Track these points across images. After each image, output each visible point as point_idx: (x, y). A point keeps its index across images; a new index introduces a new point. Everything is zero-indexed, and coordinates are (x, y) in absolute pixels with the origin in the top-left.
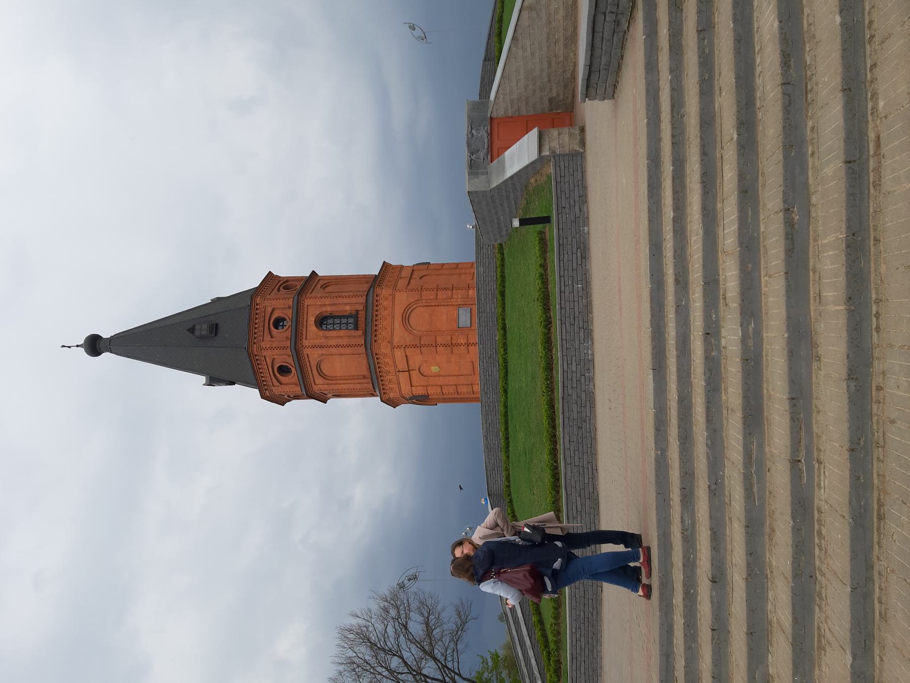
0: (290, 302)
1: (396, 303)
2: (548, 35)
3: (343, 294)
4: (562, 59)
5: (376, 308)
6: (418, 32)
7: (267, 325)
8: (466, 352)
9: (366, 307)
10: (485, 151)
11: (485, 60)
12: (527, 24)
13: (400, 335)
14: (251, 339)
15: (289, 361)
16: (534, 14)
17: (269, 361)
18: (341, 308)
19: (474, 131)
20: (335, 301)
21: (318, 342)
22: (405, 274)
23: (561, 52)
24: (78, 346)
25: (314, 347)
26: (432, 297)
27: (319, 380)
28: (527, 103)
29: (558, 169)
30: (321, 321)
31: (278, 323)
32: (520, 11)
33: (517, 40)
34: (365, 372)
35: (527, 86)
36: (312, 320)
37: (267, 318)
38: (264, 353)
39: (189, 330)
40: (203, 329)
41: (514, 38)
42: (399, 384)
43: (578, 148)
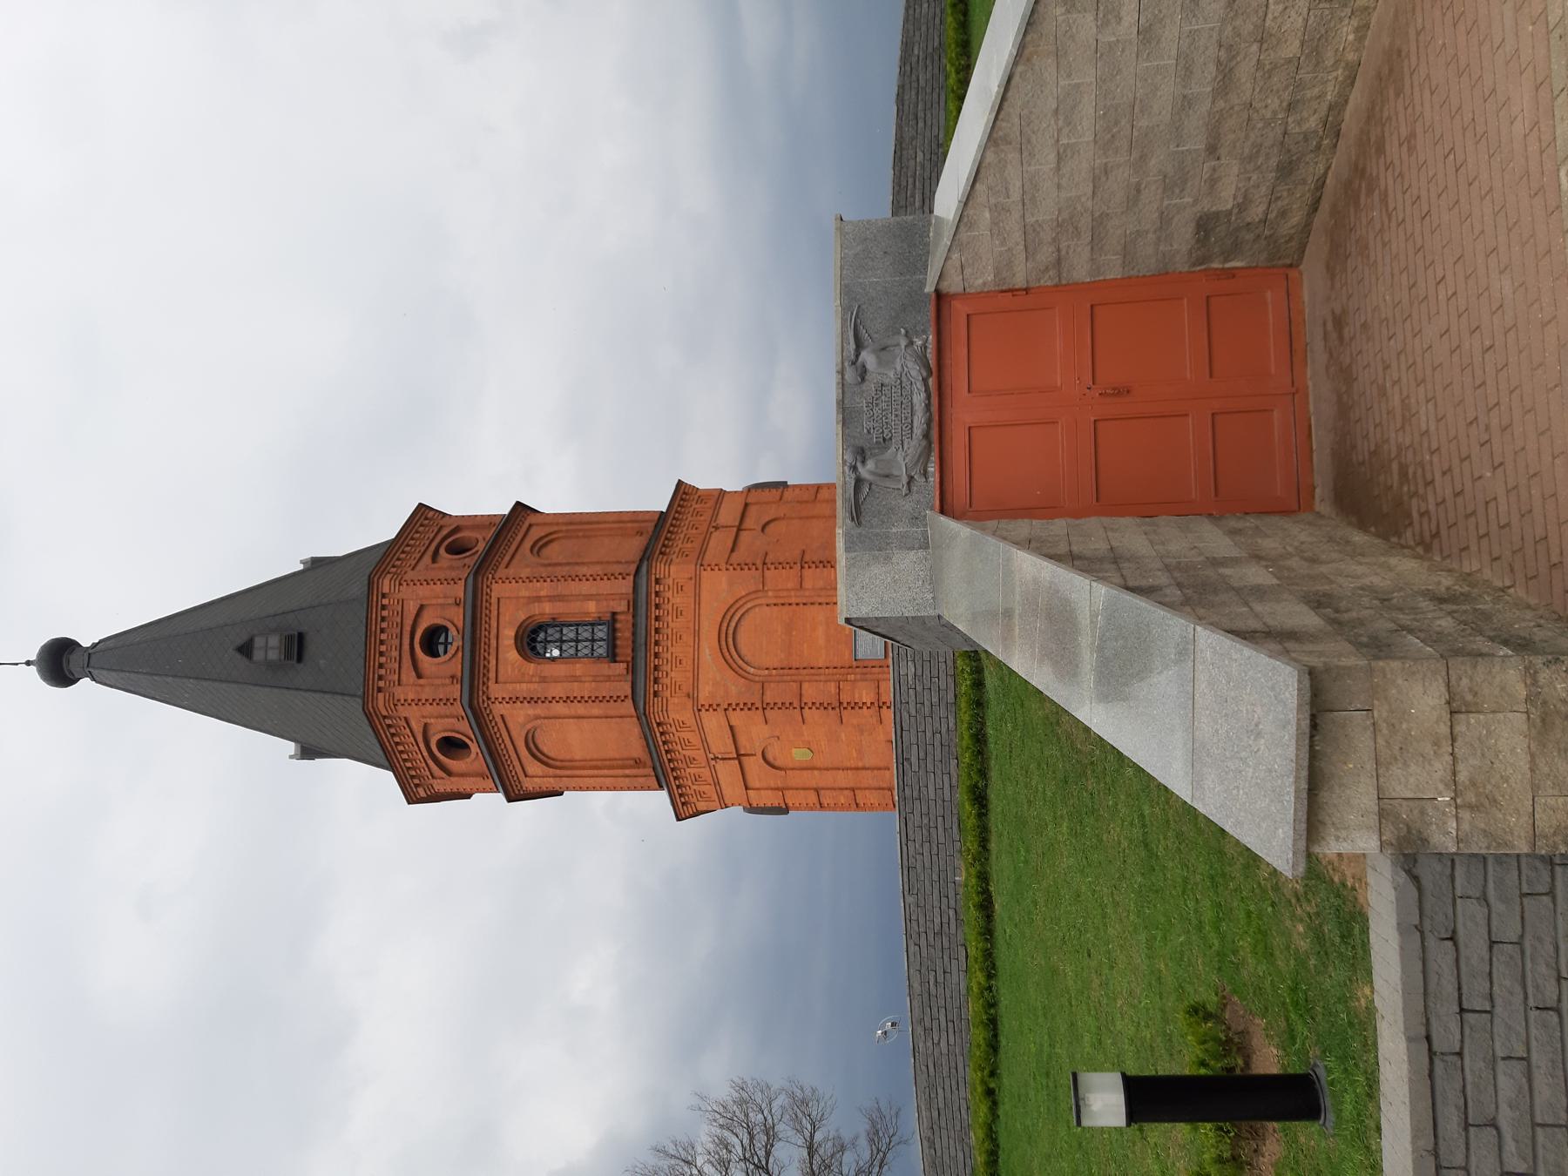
0: (458, 590)
1: (705, 595)
3: (584, 570)
4: (1291, 49)
5: (654, 612)
7: (406, 647)
8: (875, 720)
9: (634, 605)
10: (914, 445)
13: (714, 679)
14: (397, 653)
15: (463, 728)
17: (417, 728)
19: (868, 357)
21: (523, 689)
22: (728, 515)
23: (1295, 21)
24: (28, 663)
25: (514, 700)
26: (790, 585)
27: (534, 767)
28: (1096, 243)
30: (531, 640)
31: (433, 641)
34: (637, 749)
35: (1106, 171)
36: (508, 634)
37: (407, 629)
38: (404, 711)
40: (270, 648)
42: (717, 783)
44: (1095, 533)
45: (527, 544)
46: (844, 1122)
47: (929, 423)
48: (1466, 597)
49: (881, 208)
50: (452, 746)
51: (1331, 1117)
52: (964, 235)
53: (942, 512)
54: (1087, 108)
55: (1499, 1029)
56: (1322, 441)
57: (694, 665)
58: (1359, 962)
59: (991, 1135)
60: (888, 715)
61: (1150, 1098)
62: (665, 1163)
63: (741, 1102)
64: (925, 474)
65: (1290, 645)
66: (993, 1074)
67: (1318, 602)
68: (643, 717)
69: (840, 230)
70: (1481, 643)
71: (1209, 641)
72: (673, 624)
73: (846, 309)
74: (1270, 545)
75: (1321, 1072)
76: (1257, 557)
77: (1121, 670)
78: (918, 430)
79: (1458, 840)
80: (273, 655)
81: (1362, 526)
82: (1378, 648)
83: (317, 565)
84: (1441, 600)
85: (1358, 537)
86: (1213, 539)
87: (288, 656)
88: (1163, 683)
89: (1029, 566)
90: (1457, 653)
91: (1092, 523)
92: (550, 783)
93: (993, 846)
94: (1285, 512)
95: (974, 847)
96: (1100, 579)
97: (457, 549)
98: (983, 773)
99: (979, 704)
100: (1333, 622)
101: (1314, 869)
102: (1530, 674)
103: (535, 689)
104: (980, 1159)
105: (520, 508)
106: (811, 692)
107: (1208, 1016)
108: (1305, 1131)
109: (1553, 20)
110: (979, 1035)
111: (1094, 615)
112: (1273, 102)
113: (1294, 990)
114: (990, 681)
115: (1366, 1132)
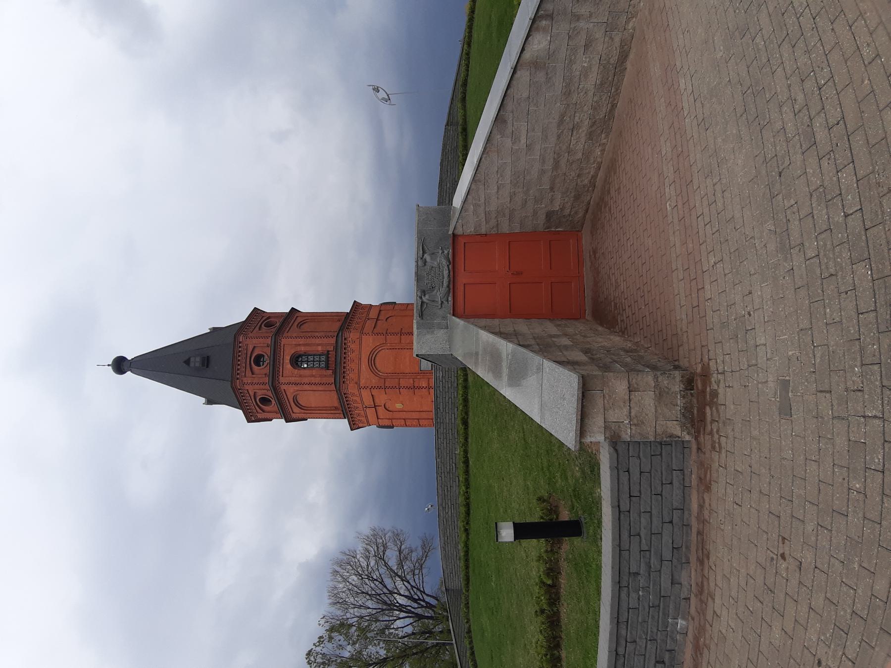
0: (269, 341)
2: (562, 116)
4: (579, 155)
6: (382, 94)
10: (444, 290)
11: (447, 124)
12: (525, 95)
13: (367, 378)
14: (246, 365)
16: (541, 76)
17: (252, 394)
18: (314, 348)
20: (309, 341)
21: (293, 379)
22: (373, 314)
23: (580, 146)
27: (296, 410)
29: (624, 478)
31: (258, 360)
32: (515, 71)
33: (505, 122)
34: (336, 404)
36: (287, 359)
37: (249, 353)
38: (246, 387)
39: (189, 359)
40: (196, 361)
41: (499, 119)
42: (366, 417)
43: (677, 431)
44: (509, 325)
45: (296, 324)
46: (413, 542)
47: (449, 282)
48: (636, 351)
49: (434, 202)
50: (265, 401)
51: (585, 535)
52: (463, 214)
53: (454, 315)
54: (508, 172)
55: (642, 502)
56: (588, 293)
57: (359, 372)
58: (597, 481)
59: (466, 545)
60: (432, 391)
61: (522, 531)
62: (345, 558)
63: (374, 535)
64: (447, 301)
65: (576, 367)
66: (467, 523)
67: (586, 352)
68: (338, 391)
69: (418, 210)
70: (640, 367)
71: (548, 364)
72: (351, 356)
73: (419, 238)
74: (570, 330)
75: (583, 520)
76: (565, 335)
77: (517, 377)
78: (445, 284)
79: (631, 437)
80: (197, 365)
81: (601, 325)
82: (606, 368)
83: (215, 330)
84: (627, 352)
85: (600, 328)
86: (550, 328)
87: (203, 365)
88: (531, 381)
89: (485, 336)
90: (632, 370)
91: (508, 321)
92: (301, 416)
93: (469, 440)
94: (576, 319)
95: (462, 440)
96: (510, 342)
97: (269, 325)
98: (467, 413)
99: (466, 387)
100: (591, 358)
101: (582, 447)
102: (656, 378)
103: (298, 380)
104: (462, 554)
105: (293, 310)
106: (403, 383)
107: (544, 501)
108: (577, 541)
109: (663, 154)
110: (463, 509)
111: (508, 355)
112: (573, 174)
113: (574, 491)
114: (470, 379)
115: (597, 539)
